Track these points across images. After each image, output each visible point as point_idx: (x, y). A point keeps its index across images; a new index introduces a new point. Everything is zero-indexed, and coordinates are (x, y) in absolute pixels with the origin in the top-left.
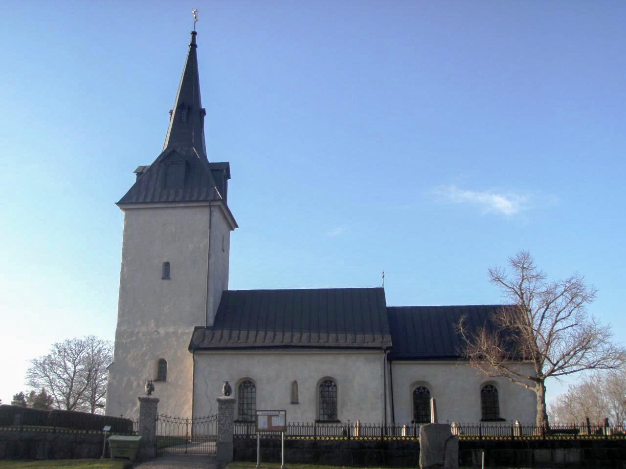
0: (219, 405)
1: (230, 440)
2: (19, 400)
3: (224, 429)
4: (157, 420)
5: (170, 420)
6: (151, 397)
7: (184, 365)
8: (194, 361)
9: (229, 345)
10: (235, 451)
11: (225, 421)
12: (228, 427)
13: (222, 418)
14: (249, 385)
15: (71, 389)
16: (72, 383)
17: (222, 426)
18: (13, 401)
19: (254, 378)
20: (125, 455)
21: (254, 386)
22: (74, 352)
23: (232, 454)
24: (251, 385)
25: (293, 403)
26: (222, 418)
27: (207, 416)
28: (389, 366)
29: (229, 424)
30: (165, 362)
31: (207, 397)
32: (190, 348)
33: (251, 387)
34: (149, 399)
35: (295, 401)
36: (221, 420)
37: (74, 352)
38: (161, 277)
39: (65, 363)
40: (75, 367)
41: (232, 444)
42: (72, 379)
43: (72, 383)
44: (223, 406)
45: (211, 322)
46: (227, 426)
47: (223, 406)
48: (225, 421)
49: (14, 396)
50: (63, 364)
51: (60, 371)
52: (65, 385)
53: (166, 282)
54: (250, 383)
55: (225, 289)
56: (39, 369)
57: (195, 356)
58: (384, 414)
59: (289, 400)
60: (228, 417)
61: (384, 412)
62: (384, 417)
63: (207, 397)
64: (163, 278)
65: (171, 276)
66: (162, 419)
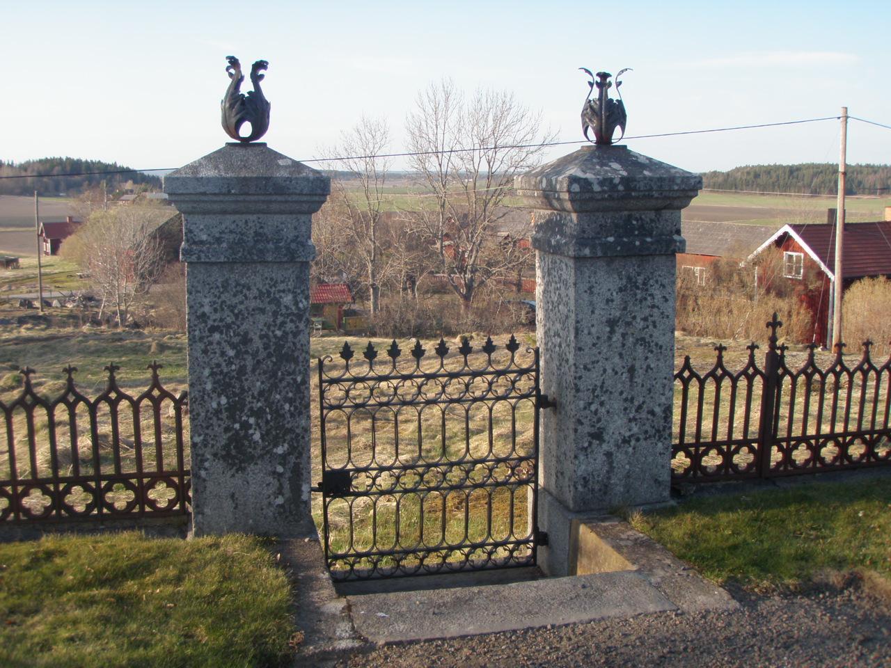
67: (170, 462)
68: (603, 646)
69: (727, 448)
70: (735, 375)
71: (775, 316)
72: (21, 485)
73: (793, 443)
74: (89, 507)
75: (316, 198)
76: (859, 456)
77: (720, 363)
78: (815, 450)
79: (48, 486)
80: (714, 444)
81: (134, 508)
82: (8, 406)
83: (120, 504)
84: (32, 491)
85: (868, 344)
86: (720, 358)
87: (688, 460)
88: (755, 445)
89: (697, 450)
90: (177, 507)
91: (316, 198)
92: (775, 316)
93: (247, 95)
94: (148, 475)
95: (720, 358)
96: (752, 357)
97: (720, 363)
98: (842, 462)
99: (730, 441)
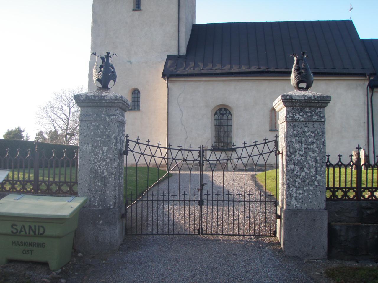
0: (288, 112)
1: (318, 202)
2: (40, 136)
3: (303, 174)
4: (126, 153)
5: (148, 152)
6: (109, 94)
7: (158, 93)
8: (168, 88)
9: (204, 71)
10: (332, 233)
11: (306, 155)
12: (313, 170)
13: (297, 146)
14: (225, 112)
15: (67, 126)
16: (68, 121)
17: (297, 168)
18: (36, 137)
19: (230, 105)
20: (34, 257)
21: (230, 113)
22: (68, 98)
23: (324, 240)
24: (226, 113)
25: (271, 130)
26: (297, 146)
27: (260, 140)
28: (371, 94)
29: (316, 162)
30: (139, 92)
31: (182, 124)
32: (163, 76)
33: (227, 114)
34: (101, 98)
35: (273, 129)
36: (294, 153)
37: (68, 98)
38: (132, 9)
39: (62, 106)
40: (70, 109)
41: (326, 213)
42: (68, 119)
43: (68, 121)
44: (297, 116)
45: (183, 51)
46: (310, 167)
47: (297, 116)
48: (306, 155)
49: (37, 134)
50: (60, 107)
51: (59, 112)
52: (63, 123)
53: (137, 13)
54: (226, 110)
55: (194, 24)
56: (42, 112)
57: (168, 84)
58: (366, 143)
59: (267, 127)
60: (313, 143)
61: (367, 140)
62: (367, 145)
63: (182, 124)
64: (133, 10)
65: (142, 8)
66: (137, 149)
67: (343, 185)
68: (301, 249)
69: (346, 191)
70: (334, 165)
71: (359, 146)
72: (347, 188)
73: (25, 182)
74: (343, 196)
75: (327, 102)
76: (375, 195)
77: (340, 161)
78: (345, 193)
79: (347, 190)
80: (340, 188)
81: (26, 190)
82: (346, 165)
83: (366, 196)
84: (366, 190)
85: (340, 156)
86: (340, 159)
87: (5, 186)
88: (355, 189)
89: (334, 190)
90: (22, 191)
91: (327, 102)
92: (359, 146)
93: (217, 64)
94: (348, 188)
95: (340, 159)
96: (351, 159)
97: (340, 161)
98: (13, 190)
99: (346, 188)
